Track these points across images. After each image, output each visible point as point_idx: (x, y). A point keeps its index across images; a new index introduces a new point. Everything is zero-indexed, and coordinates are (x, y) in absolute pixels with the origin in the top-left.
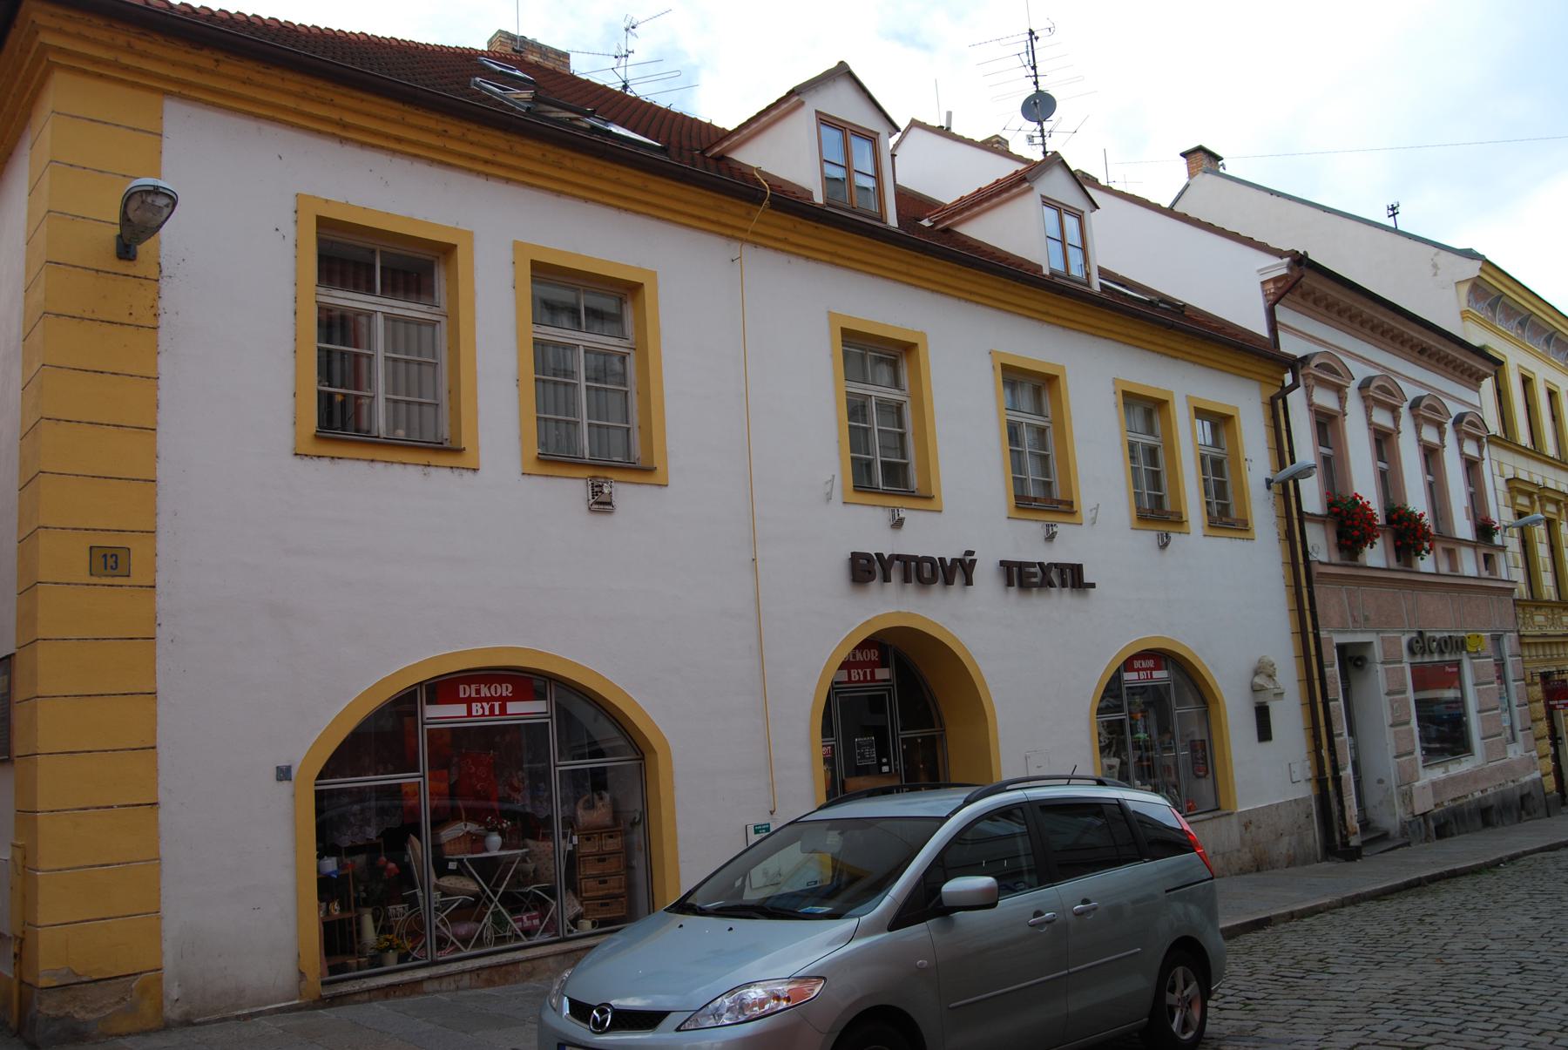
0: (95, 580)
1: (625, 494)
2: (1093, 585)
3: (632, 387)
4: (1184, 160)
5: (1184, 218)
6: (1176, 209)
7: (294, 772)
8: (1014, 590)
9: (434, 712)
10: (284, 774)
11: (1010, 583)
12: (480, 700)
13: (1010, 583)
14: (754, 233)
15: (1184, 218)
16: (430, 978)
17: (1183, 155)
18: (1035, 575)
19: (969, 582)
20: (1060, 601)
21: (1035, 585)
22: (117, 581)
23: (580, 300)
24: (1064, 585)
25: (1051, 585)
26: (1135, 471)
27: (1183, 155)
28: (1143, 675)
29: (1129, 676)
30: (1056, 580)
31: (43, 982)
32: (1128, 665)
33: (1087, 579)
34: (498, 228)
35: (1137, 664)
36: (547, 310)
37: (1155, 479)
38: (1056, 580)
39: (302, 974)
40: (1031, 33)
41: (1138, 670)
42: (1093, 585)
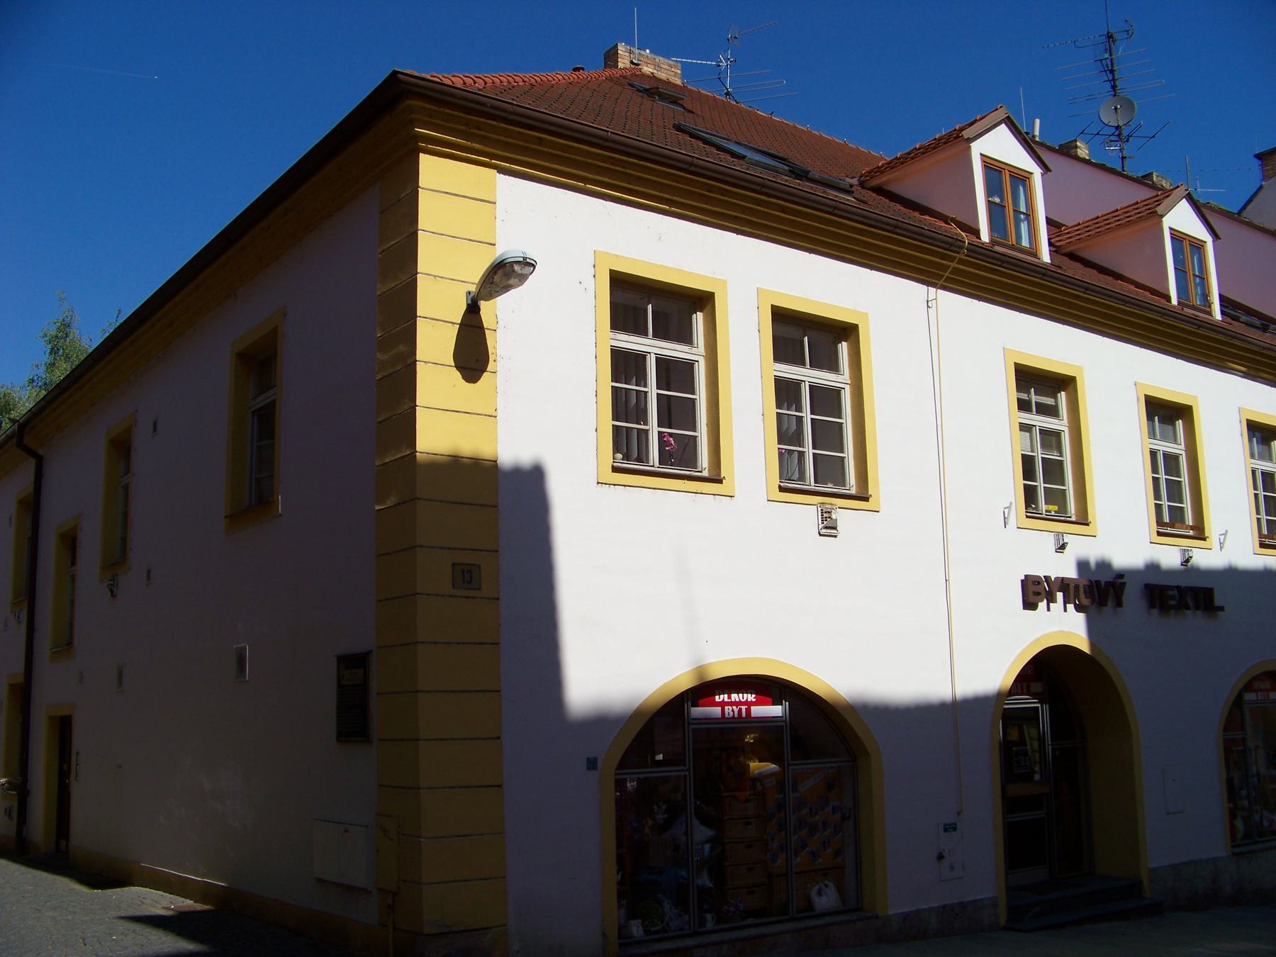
0: (455, 592)
1: (845, 516)
2: (1222, 609)
3: (847, 420)
4: (1257, 162)
5: (1250, 225)
6: (1249, 214)
7: (599, 765)
8: (1155, 612)
9: (698, 711)
10: (592, 764)
11: (1152, 606)
12: (731, 704)
13: (1152, 606)
14: (955, 271)
15: (1250, 225)
16: (699, 946)
17: (1257, 156)
18: (1172, 598)
19: (1119, 603)
20: (1194, 619)
21: (1173, 607)
22: (472, 593)
23: (806, 336)
24: (1197, 608)
25: (1187, 608)
26: (1156, 481)
27: (1257, 156)
28: (1261, 696)
29: (1249, 696)
30: (1190, 603)
31: (427, 930)
32: (1248, 687)
33: (1217, 603)
34: (749, 275)
35: (1256, 685)
36: (784, 350)
37: (1175, 491)
38: (1190, 603)
39: (604, 935)
40: (1110, 37)
41: (1256, 691)
42: (1222, 609)
